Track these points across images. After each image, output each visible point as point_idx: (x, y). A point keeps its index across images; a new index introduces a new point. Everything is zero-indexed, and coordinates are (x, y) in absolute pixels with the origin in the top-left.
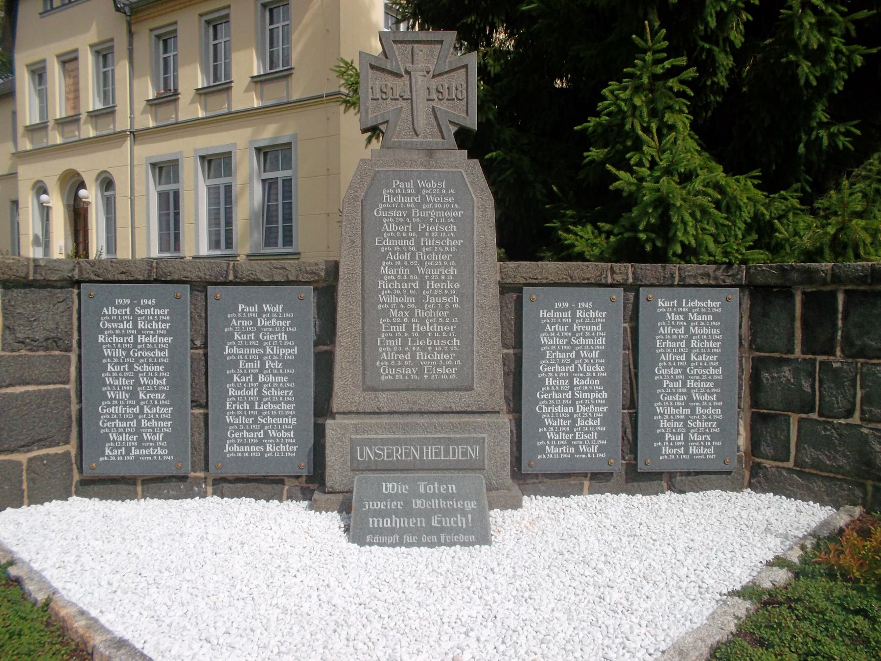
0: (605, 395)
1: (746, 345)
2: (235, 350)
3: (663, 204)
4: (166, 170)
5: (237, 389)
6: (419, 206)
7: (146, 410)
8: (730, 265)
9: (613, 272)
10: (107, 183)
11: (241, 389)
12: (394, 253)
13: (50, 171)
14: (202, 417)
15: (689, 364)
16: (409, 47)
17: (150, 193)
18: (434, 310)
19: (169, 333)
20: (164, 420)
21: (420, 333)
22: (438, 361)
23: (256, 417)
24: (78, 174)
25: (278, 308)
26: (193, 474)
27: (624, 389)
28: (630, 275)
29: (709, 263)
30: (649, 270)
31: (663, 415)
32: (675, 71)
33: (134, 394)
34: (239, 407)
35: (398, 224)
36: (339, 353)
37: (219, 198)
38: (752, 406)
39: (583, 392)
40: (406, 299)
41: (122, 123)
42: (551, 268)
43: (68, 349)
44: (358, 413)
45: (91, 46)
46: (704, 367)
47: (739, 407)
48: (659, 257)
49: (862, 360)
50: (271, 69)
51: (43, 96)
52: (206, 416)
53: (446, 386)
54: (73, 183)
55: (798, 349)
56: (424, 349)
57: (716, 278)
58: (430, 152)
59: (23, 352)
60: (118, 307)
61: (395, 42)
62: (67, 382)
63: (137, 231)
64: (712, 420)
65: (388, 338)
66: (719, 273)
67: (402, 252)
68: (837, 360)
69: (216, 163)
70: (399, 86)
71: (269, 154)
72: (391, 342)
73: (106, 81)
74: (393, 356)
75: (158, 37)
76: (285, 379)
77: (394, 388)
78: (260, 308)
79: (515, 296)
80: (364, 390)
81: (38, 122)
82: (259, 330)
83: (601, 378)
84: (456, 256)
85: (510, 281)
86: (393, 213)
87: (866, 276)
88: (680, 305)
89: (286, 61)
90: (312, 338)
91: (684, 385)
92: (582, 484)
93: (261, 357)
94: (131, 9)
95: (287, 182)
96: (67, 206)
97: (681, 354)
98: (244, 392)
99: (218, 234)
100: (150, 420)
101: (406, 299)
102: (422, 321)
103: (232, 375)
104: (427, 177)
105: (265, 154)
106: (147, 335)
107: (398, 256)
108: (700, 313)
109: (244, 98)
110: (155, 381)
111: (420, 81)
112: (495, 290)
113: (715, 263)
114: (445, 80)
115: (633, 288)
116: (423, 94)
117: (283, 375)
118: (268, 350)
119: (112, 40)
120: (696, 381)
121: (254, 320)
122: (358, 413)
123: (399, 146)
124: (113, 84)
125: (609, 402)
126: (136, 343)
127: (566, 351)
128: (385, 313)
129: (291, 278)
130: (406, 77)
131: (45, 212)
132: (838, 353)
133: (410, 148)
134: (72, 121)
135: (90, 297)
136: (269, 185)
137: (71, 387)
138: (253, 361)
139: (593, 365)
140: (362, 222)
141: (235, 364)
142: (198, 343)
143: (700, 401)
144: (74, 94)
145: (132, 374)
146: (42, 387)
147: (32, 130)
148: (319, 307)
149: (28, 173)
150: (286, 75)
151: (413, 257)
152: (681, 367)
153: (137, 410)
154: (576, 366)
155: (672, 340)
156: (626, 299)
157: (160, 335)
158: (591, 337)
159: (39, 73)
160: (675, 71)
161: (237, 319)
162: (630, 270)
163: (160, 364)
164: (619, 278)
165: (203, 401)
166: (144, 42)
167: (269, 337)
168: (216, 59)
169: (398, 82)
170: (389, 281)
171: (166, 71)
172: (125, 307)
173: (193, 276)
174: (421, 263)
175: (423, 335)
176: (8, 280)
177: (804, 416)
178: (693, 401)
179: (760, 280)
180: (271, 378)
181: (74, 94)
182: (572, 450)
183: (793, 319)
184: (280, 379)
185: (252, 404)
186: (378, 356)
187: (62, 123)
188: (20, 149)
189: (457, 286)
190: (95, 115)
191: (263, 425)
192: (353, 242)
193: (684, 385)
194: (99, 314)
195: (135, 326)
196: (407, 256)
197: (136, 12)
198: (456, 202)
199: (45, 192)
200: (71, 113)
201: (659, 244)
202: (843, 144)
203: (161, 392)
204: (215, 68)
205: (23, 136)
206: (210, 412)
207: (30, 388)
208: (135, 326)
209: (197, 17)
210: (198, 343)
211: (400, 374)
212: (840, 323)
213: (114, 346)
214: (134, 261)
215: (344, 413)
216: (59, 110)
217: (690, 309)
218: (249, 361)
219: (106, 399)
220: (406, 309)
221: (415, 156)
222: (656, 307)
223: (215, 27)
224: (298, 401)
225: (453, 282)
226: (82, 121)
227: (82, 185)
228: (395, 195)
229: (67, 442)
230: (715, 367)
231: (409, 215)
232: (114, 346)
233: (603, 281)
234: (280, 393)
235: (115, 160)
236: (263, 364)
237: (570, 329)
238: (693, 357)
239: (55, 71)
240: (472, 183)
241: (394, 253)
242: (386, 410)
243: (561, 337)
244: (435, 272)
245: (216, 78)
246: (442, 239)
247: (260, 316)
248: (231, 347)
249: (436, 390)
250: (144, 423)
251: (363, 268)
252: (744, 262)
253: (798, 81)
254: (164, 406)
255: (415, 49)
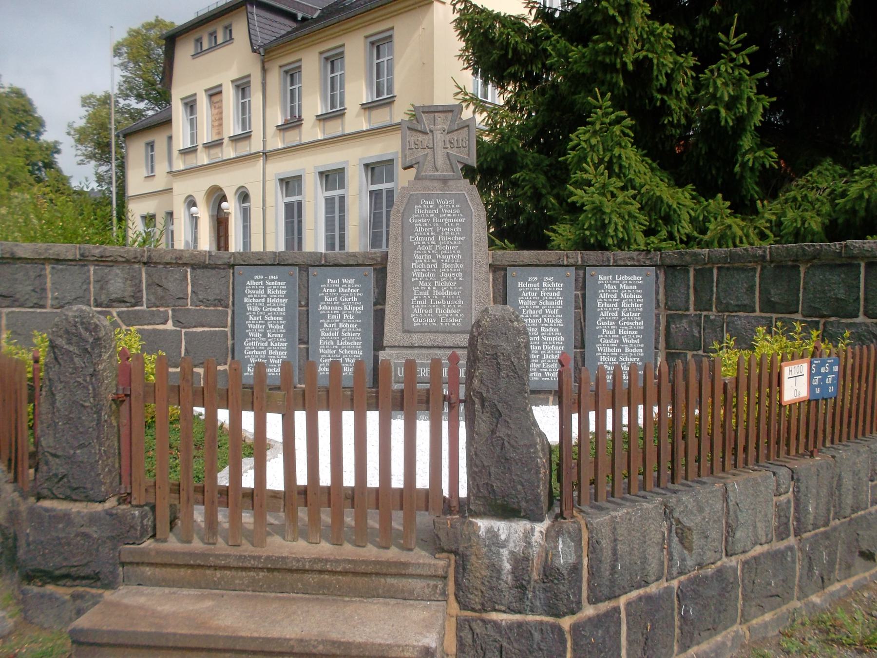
0: (562, 339)
1: (662, 305)
2: (325, 307)
3: (598, 210)
4: (291, 184)
5: (326, 332)
6: (437, 216)
7: (272, 344)
8: (649, 251)
9: (568, 257)
10: (244, 196)
11: (328, 332)
12: (421, 245)
13: (198, 186)
14: (305, 350)
15: (620, 319)
16: (432, 115)
17: (278, 201)
18: (447, 282)
19: (286, 297)
20: (282, 350)
21: (438, 296)
22: (449, 314)
23: (337, 350)
24: (221, 189)
25: (352, 281)
26: (299, 386)
27: (575, 335)
28: (579, 259)
29: (635, 250)
30: (593, 256)
31: (602, 353)
32: (618, 121)
33: (264, 335)
34: (327, 343)
35: (424, 227)
36: (388, 308)
37: (334, 207)
38: (667, 348)
39: (548, 336)
40: (429, 275)
41: (256, 145)
42: (527, 255)
43: (227, 307)
44: (399, 347)
45: (233, 81)
46: (630, 321)
47: (656, 348)
48: (601, 246)
49: (727, 314)
50: (378, 96)
51: (193, 123)
52: (307, 349)
53: (455, 330)
54: (217, 196)
55: (692, 307)
56: (440, 306)
57: (638, 261)
58: (445, 181)
59: (202, 307)
60: (256, 281)
61: (423, 112)
62: (226, 327)
63: (268, 236)
64: (637, 357)
65: (418, 299)
66: (641, 257)
67: (427, 245)
68: (713, 314)
69: (332, 178)
70: (425, 139)
71: (375, 169)
72: (420, 302)
73: (244, 109)
74: (421, 311)
75: (286, 72)
76: (356, 326)
77: (421, 331)
78: (341, 281)
79: (503, 273)
80: (403, 332)
81: (190, 146)
82: (340, 295)
83: (560, 328)
84: (460, 247)
85: (498, 263)
86: (421, 220)
87: (726, 257)
88: (614, 278)
89: (390, 90)
90: (372, 301)
91: (617, 332)
92: (548, 399)
93: (341, 312)
94: (265, 50)
95: (390, 192)
96: (212, 216)
97: (615, 312)
98: (330, 334)
99: (333, 237)
100: (274, 351)
101: (429, 275)
102: (439, 289)
103: (323, 323)
104: (442, 197)
105: (373, 169)
106: (273, 298)
107: (424, 248)
108: (628, 284)
109: (355, 121)
110: (277, 327)
111: (439, 136)
112: (486, 268)
113: (639, 250)
114: (455, 136)
115: (581, 267)
116: (441, 144)
117: (355, 323)
118: (345, 308)
119: (249, 76)
120: (625, 330)
121: (337, 288)
122: (399, 347)
123: (425, 178)
124: (250, 113)
125: (565, 343)
126: (266, 303)
127: (536, 309)
128: (416, 283)
129: (360, 262)
130: (430, 134)
131: (194, 220)
132: (714, 309)
133: (432, 179)
134: (216, 144)
135: (240, 275)
136: (375, 196)
137: (228, 329)
138: (335, 314)
139: (554, 318)
140: (402, 226)
141: (325, 316)
142: (303, 303)
143: (628, 344)
144: (218, 122)
145: (263, 322)
146: (212, 329)
147: (185, 152)
148: (377, 281)
149: (182, 188)
150: (389, 102)
151: (433, 248)
152: (614, 320)
153: (266, 344)
154: (543, 319)
155: (608, 302)
156: (577, 275)
157: (280, 298)
158: (553, 300)
159: (190, 104)
160: (618, 121)
161: (327, 288)
162: (580, 256)
163: (280, 316)
164: (572, 261)
165: (305, 339)
166: (275, 78)
167: (346, 299)
168: (333, 89)
169: (426, 137)
170: (419, 263)
171: (292, 101)
172: (260, 280)
173: (300, 261)
174: (439, 251)
175: (440, 298)
176: (194, 264)
177: (695, 353)
178: (623, 343)
179: (668, 261)
180: (347, 325)
181: (218, 122)
182: (540, 375)
183: (689, 288)
184: (352, 326)
185: (335, 341)
186: (411, 311)
187: (208, 146)
188: (174, 169)
189: (462, 266)
190: (235, 139)
191: (342, 355)
192: (396, 239)
193: (617, 332)
194: (245, 285)
195: (266, 293)
196: (429, 248)
197: (269, 52)
198: (461, 212)
199: (195, 205)
200: (216, 138)
201: (599, 238)
202: (770, 165)
203: (281, 333)
204: (332, 97)
205: (177, 158)
206: (310, 346)
207: (206, 329)
208: (266, 293)
209: (317, 55)
210: (303, 303)
211: (425, 322)
212: (715, 289)
213: (253, 304)
214: (264, 253)
215: (391, 347)
216: (205, 135)
217: (621, 281)
218: (334, 314)
219: (248, 337)
220: (429, 281)
221: (436, 184)
222: (597, 280)
223: (332, 62)
224: (364, 340)
225: (459, 263)
226: (224, 144)
227: (224, 198)
228: (423, 209)
229: (225, 364)
230: (638, 321)
231: (431, 222)
232: (253, 304)
233: (561, 263)
234: (353, 335)
235: (249, 176)
236: (342, 316)
237: (539, 295)
238: (623, 314)
239: (203, 103)
240: (472, 200)
241: (421, 245)
242: (417, 345)
243: (532, 300)
244: (447, 257)
245: (333, 106)
246: (451, 236)
247: (340, 286)
248: (323, 305)
249: (449, 333)
250: (270, 352)
251: (402, 255)
252: (660, 249)
253: (720, 122)
254: (283, 342)
255: (437, 117)
